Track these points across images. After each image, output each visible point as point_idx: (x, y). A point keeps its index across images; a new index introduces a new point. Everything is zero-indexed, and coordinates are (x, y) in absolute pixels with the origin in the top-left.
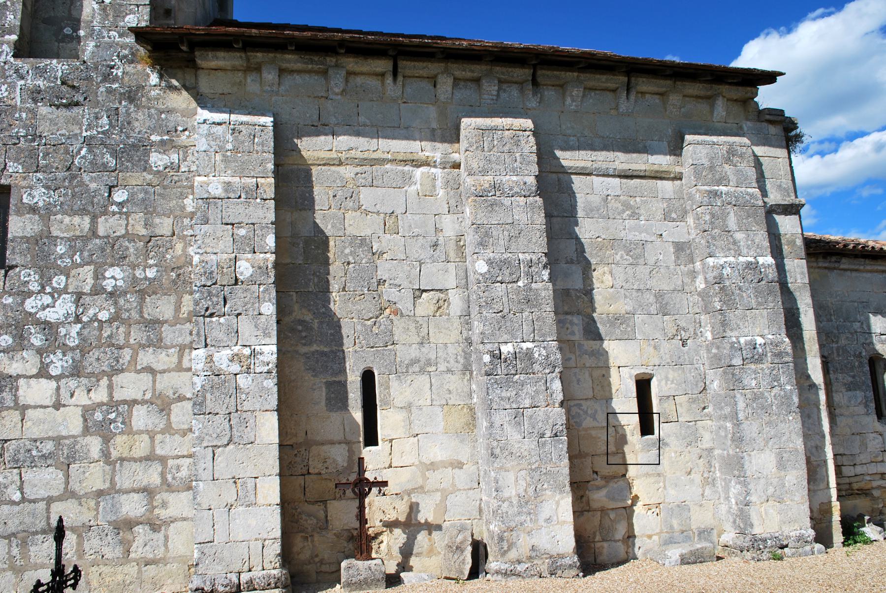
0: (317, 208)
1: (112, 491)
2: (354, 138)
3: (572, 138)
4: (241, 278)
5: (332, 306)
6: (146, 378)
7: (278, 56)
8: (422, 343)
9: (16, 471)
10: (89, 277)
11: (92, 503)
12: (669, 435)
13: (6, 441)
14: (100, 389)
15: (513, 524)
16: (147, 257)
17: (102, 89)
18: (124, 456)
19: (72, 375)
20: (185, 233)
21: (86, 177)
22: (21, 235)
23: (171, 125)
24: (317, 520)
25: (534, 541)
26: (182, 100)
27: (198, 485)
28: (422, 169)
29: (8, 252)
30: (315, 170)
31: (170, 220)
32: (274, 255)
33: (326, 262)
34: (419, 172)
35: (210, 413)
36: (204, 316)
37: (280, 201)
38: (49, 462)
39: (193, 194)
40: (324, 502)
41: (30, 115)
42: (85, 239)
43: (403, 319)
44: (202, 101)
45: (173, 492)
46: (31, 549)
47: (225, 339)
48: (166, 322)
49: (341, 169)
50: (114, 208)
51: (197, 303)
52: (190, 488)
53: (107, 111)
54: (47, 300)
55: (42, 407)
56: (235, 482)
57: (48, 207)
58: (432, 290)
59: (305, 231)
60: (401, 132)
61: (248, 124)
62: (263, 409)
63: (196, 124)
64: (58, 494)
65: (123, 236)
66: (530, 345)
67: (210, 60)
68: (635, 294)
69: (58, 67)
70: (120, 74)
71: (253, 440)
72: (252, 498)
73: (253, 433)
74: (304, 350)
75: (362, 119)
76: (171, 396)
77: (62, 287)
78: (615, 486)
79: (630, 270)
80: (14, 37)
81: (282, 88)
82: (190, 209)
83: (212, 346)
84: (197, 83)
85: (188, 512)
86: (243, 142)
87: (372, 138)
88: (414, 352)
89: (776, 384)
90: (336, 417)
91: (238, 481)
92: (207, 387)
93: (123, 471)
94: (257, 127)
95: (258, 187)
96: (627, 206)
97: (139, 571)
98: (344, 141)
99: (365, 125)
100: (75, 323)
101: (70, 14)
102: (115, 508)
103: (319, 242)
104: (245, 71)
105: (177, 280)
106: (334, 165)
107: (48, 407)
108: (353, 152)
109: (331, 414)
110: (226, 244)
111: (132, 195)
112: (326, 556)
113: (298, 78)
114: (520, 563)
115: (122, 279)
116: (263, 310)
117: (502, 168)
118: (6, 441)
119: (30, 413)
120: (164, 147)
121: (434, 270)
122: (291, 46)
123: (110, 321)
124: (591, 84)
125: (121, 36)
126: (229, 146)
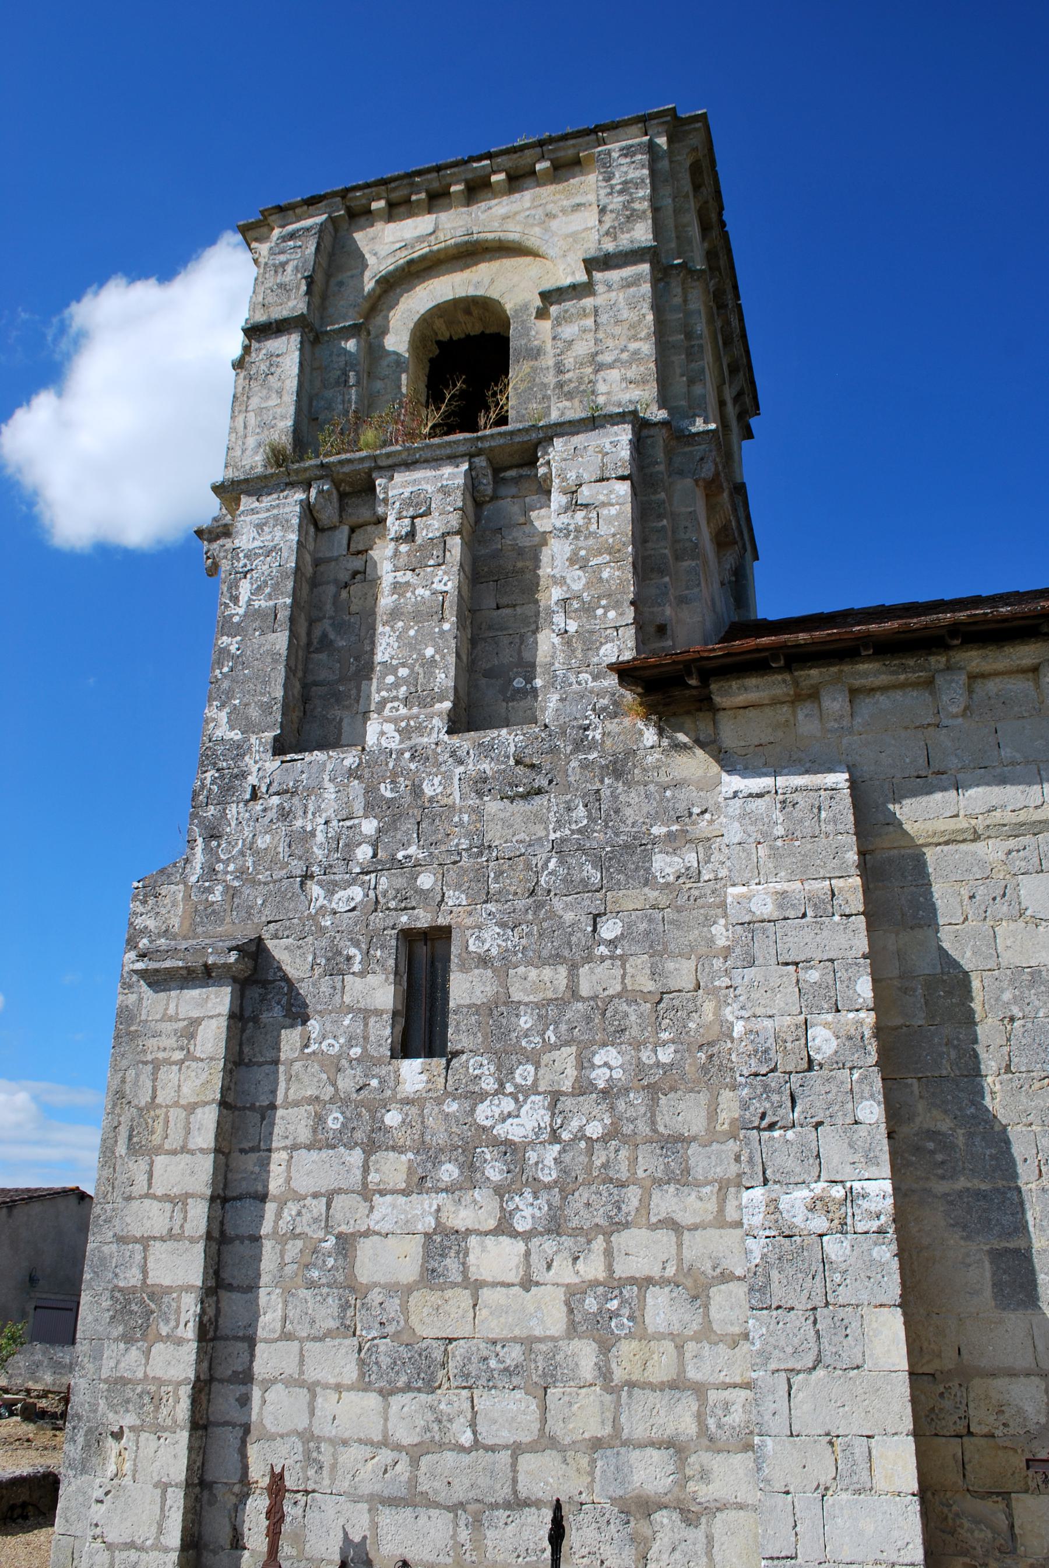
0: (941, 921)
2: (996, 790)
4: (817, 1057)
5: (987, 1101)
6: (666, 1238)
7: (846, 668)
9: (465, 1393)
10: (569, 1065)
11: (584, 1461)
13: (451, 1340)
14: (592, 1257)
16: (658, 1028)
17: (574, 764)
18: (634, 1379)
19: (549, 1232)
20: (717, 983)
21: (558, 904)
22: (468, 1002)
23: (682, 807)
24: (993, 1531)
26: (696, 764)
27: (763, 1444)
29: (450, 1031)
30: (931, 855)
31: (692, 963)
32: (872, 1013)
33: (969, 1020)
35: (779, 1307)
36: (758, 1128)
37: (876, 915)
38: (516, 1380)
39: (725, 916)
40: (1006, 1495)
41: (474, 817)
42: (561, 1003)
44: (728, 761)
45: (719, 1452)
47: (798, 1169)
48: (694, 1139)
49: (979, 847)
50: (603, 950)
51: (745, 1106)
52: (749, 1447)
53: (583, 797)
56: (831, 1443)
57: (505, 956)
59: (925, 966)
61: (806, 789)
62: (874, 1302)
63: (721, 799)
64: (528, 1439)
65: (619, 996)
67: (734, 694)
69: (508, 739)
70: (598, 737)
71: (859, 1362)
72: (865, 1476)
73: (860, 1348)
74: (942, 1187)
75: (1006, 753)
76: (710, 1272)
77: (529, 1083)
80: (447, 705)
81: (858, 720)
82: (721, 942)
83: (775, 1182)
84: (717, 734)
85: (748, 1494)
86: (801, 821)
87: (1030, 784)
90: (1015, 1320)
91: (838, 1442)
92: (772, 1258)
94: (822, 792)
95: (833, 895)
98: (978, 798)
99: (1013, 763)
100: (550, 1143)
101: (520, 658)
102: (621, 1473)
103: (952, 984)
104: (793, 702)
105: (709, 1066)
106: (964, 841)
108: (997, 814)
109: (1005, 1314)
110: (786, 998)
111: (629, 926)
113: (883, 700)
115: (621, 1066)
116: (860, 1116)
118: (451, 1340)
119: (485, 1293)
120: (674, 842)
122: (866, 648)
123: (605, 1139)
125: (595, 678)
126: (779, 831)
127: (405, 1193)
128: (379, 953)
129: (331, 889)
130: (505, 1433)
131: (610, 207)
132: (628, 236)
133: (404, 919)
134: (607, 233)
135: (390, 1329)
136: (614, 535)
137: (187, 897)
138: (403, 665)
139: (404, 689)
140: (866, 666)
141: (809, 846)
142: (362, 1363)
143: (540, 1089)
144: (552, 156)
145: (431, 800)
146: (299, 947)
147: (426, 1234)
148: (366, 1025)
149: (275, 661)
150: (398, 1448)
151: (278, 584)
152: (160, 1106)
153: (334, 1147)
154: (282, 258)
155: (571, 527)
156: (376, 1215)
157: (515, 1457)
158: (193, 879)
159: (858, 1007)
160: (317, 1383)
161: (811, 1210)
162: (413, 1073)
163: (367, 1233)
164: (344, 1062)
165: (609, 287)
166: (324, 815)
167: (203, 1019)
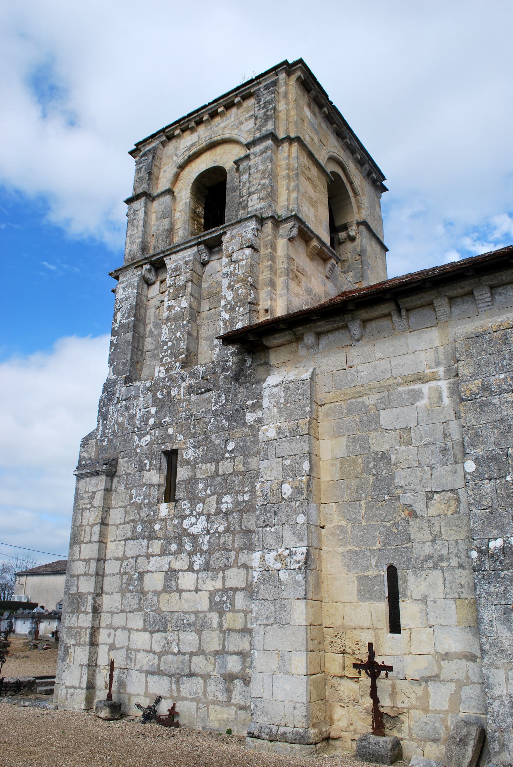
1: (221, 653)
6: (243, 571)
9: (176, 633)
14: (218, 579)
15: (504, 725)
17: (222, 377)
18: (230, 627)
19: (205, 570)
22: (182, 479)
29: (176, 491)
34: (425, 388)
36: (262, 527)
38: (193, 628)
41: (187, 403)
42: (212, 477)
43: (418, 520)
50: (227, 455)
53: (224, 391)
58: (443, 491)
65: (232, 473)
70: (231, 365)
77: (201, 511)
88: (428, 549)
92: (261, 579)
93: (230, 639)
94: (300, 382)
97: (236, 712)
100: (207, 535)
107: (192, 591)
111: (237, 445)
112: (359, 728)
115: (231, 503)
117: (491, 369)
123: (224, 532)
127: (160, 556)
128: (155, 462)
129: (140, 437)
131: (259, 116)
132: (265, 129)
133: (163, 447)
134: (257, 129)
135: (154, 608)
136: (244, 274)
137: (96, 443)
138: (170, 341)
139: (170, 351)
140: (320, 323)
141: (293, 406)
142: (145, 621)
143: (204, 513)
144: (241, 95)
146: (130, 461)
147: (166, 572)
148: (150, 490)
149: (128, 345)
150: (155, 653)
151: (129, 312)
152: (83, 526)
153: (138, 539)
154: (141, 166)
155: (229, 273)
156: (150, 565)
157: (190, 657)
158: (99, 437)
159: (303, 474)
160: (131, 629)
161: (276, 560)
162: (164, 509)
163: (148, 572)
164: (143, 505)
165: (256, 156)
166: (139, 407)
167: (96, 491)
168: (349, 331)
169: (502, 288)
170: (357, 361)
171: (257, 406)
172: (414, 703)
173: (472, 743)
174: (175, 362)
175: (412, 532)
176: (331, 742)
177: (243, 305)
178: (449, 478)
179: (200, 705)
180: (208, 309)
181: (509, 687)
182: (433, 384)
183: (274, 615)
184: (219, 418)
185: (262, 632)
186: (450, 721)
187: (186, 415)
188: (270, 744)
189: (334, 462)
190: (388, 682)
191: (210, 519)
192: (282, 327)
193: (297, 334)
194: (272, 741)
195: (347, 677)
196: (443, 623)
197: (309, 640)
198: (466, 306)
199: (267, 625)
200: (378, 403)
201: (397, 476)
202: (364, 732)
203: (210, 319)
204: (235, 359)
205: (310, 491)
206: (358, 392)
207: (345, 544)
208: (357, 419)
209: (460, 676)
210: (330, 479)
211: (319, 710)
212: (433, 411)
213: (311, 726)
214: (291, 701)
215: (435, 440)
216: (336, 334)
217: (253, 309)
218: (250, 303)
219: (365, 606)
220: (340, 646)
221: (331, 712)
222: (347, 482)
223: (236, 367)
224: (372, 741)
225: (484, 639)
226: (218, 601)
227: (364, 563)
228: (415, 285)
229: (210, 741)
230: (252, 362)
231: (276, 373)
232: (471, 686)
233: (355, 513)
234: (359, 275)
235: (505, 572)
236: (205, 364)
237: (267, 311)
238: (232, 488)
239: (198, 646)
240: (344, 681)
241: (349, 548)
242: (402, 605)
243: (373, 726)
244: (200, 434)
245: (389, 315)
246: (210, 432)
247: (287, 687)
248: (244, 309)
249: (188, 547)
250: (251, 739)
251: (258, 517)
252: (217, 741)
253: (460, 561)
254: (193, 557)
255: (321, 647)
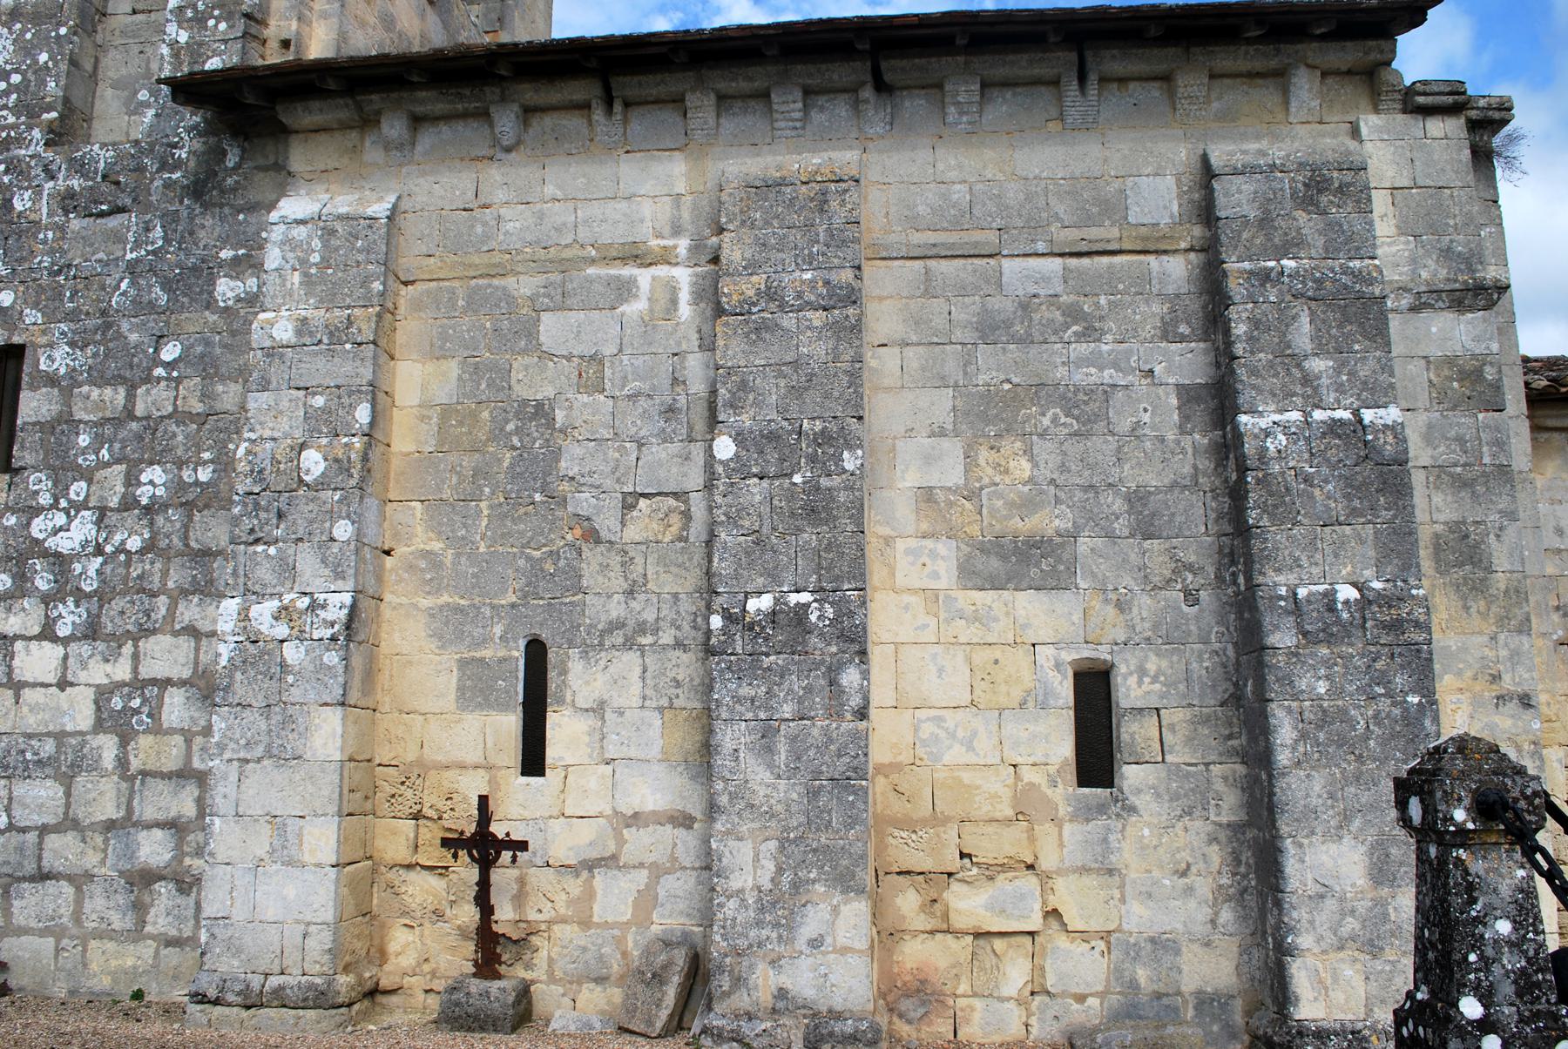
1: (123, 826)
3: (957, 187)
6: (186, 644)
7: (405, 95)
8: (631, 592)
12: (1139, 791)
14: (121, 660)
15: (742, 943)
18: (148, 767)
19: (86, 637)
22: (34, 419)
25: (785, 981)
28: (653, 270)
34: (644, 277)
38: (48, 771)
41: (58, 234)
42: (118, 422)
43: (601, 548)
46: (15, 903)
50: (159, 371)
53: (161, 218)
54: (60, 519)
55: (43, 685)
60: (618, 206)
65: (169, 416)
66: (805, 597)
68: (1079, 495)
70: (184, 156)
78: (1009, 887)
79: (1074, 448)
86: (337, 249)
88: (616, 609)
89: (1380, 690)
96: (1073, 314)
102: (130, 852)
111: (186, 350)
112: (443, 965)
114: (750, 1019)
116: (336, 533)
117: (788, 257)
119: (27, 693)
120: (238, 267)
121: (663, 455)
123: (142, 552)
124: (1001, 72)
130: (36, 817)
138: (16, 71)
139: (14, 96)
145: (20, 214)
157: (41, 836)
161: (276, 619)
168: (491, 126)
169: (825, 98)
170: (500, 195)
171: (249, 264)
172: (562, 911)
173: (676, 979)
174: (30, 128)
175: (586, 573)
176: (380, 998)
177: (228, 17)
178: (674, 470)
179: (65, 942)
180: (129, 10)
181: (759, 872)
182: (662, 271)
183: (265, 739)
184: (142, 282)
185: (233, 777)
186: (634, 944)
187: (53, 264)
188: (245, 1014)
189: (425, 412)
190: (513, 873)
191: (106, 521)
192: (332, 85)
193: (366, 109)
194: (248, 1007)
195: (423, 867)
196: (633, 755)
197: (346, 791)
198: (749, 120)
199: (247, 761)
200: (538, 295)
201: (565, 456)
202: (455, 974)
203: (134, 37)
204: (197, 145)
205: (369, 471)
206: (495, 265)
207: (437, 592)
208: (488, 325)
209: (658, 856)
210: (413, 448)
211: (358, 937)
212: (654, 327)
213: (340, 969)
214: (298, 922)
215: (653, 388)
216: (460, 126)
217: (253, 31)
218: (248, 16)
219: (473, 721)
220: (410, 803)
221: (382, 938)
222: (453, 458)
223: (199, 164)
224: (473, 989)
225: (719, 786)
226: (119, 708)
227: (477, 632)
228: (653, 50)
229: (95, 1019)
230: (242, 158)
231: (302, 192)
232: (678, 874)
233: (465, 526)
234: (494, 16)
235: (772, 658)
236: (114, 144)
237: (286, 44)
238: (169, 450)
239: (61, 811)
240: (414, 876)
241: (446, 598)
242: (551, 719)
243: (476, 961)
244: (88, 314)
245: (585, 107)
246: (117, 311)
247: (291, 892)
248: (231, 27)
249: (43, 583)
250: (199, 1007)
251: (235, 522)
252: (112, 1017)
253: (678, 634)
254: (56, 607)
255: (368, 806)
